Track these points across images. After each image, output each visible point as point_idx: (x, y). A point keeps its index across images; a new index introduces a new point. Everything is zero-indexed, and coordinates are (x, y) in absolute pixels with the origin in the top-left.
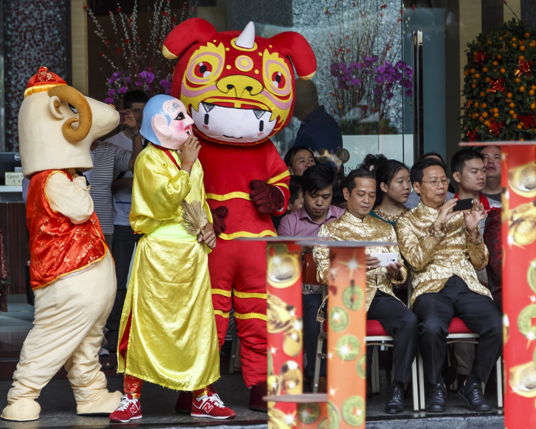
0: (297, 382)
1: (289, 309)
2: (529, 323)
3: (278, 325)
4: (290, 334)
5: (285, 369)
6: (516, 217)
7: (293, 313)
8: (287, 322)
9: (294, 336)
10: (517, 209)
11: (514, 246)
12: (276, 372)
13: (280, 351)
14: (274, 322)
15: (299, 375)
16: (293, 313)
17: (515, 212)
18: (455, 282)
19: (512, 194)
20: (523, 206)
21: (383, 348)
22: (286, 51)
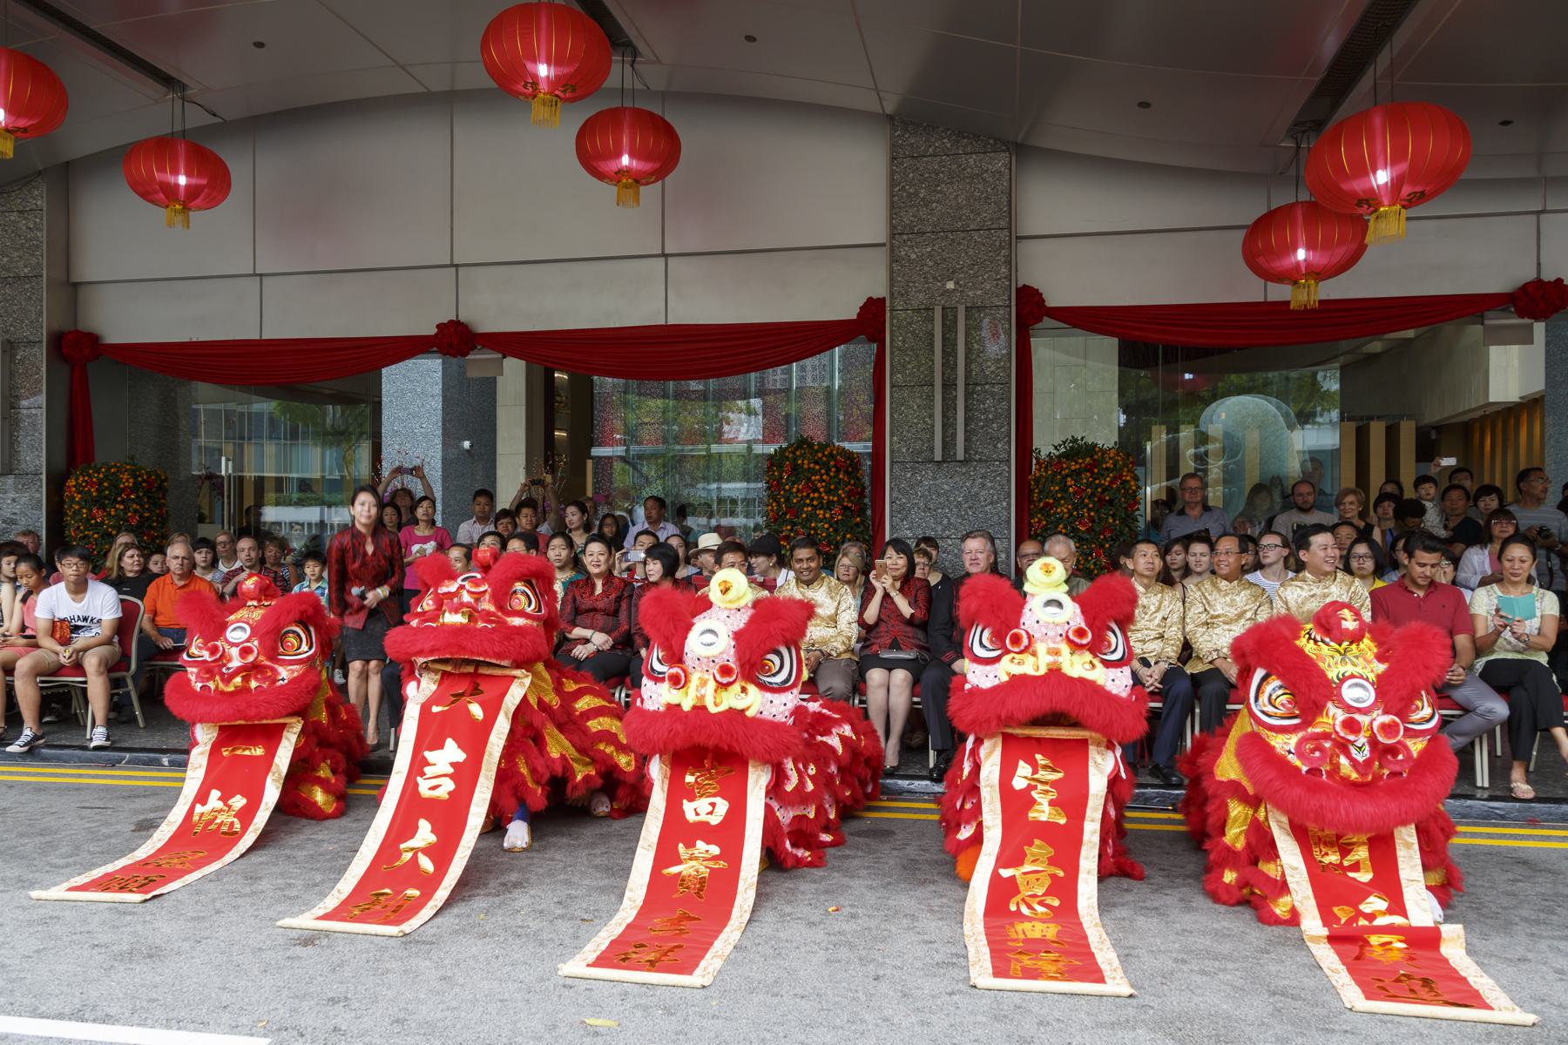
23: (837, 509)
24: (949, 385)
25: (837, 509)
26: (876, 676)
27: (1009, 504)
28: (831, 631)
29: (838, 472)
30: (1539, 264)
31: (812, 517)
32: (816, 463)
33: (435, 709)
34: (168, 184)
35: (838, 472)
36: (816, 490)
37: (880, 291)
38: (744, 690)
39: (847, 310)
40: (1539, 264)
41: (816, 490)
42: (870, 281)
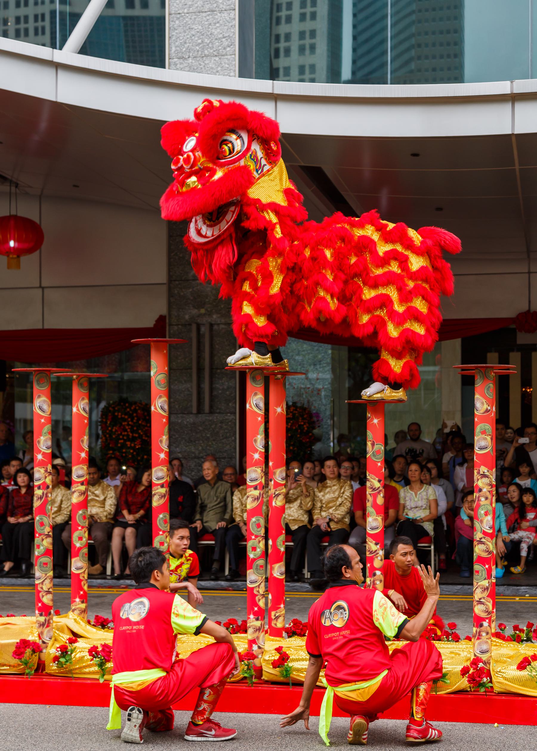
0: (381, 581)
1: (376, 544)
2: (77, 539)
3: (371, 552)
4: (377, 557)
5: (375, 575)
6: (277, 493)
7: (378, 546)
8: (376, 551)
9: (379, 558)
10: (277, 489)
11: (275, 507)
12: (370, 576)
13: (372, 565)
14: (369, 551)
15: (382, 578)
16: (378, 546)
17: (276, 490)
18: (130, 512)
19: (275, 482)
20: (280, 488)
21: (506, 563)
22: (238, 347)
23: (138, 441)
24: (200, 370)
25: (138, 441)
26: (117, 531)
27: (235, 438)
28: (101, 510)
29: (138, 420)
30: (530, 302)
31: (124, 446)
32: (126, 414)
33: (327, 544)
34: (253, 290)
35: (138, 420)
36: (125, 430)
37: (164, 311)
38: (167, 537)
39: (149, 322)
40: (530, 302)
41: (125, 430)
42: (160, 307)
